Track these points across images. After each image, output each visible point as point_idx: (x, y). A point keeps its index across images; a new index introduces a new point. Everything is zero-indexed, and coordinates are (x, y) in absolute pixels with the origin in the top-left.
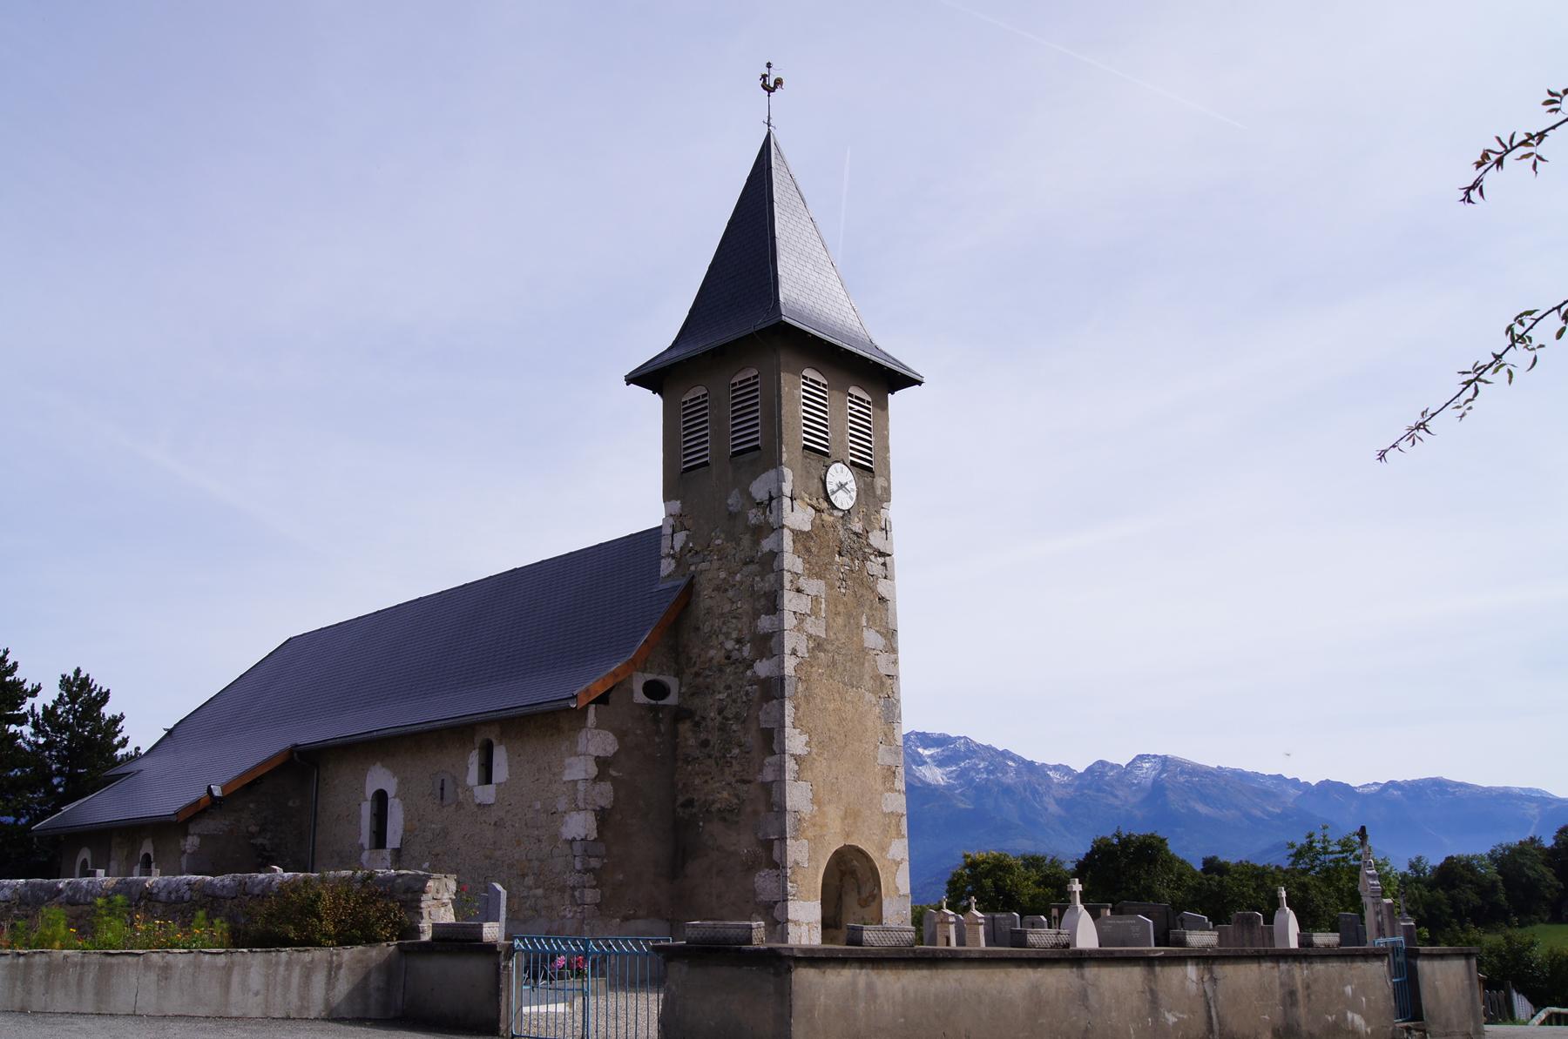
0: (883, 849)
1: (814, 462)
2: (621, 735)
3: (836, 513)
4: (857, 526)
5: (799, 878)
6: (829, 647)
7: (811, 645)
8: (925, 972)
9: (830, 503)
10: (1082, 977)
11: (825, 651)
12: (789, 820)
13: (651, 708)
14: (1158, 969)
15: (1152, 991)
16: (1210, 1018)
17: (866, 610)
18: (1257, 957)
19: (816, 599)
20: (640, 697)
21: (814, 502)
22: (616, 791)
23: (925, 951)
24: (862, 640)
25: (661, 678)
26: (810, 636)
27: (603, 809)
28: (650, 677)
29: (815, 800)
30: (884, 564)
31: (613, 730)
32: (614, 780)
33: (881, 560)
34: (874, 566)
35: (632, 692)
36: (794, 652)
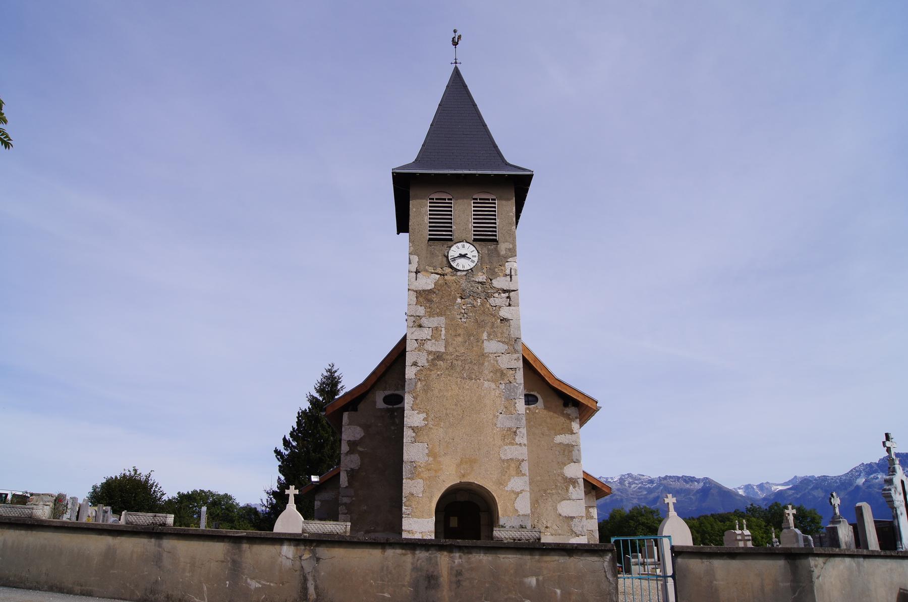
0: (501, 483)
1: (438, 247)
2: (366, 427)
3: (459, 273)
4: (481, 277)
5: (414, 504)
6: (448, 357)
7: (431, 357)
8: (23, 532)
9: (451, 267)
10: (160, 546)
11: (443, 360)
12: (406, 469)
13: (388, 410)
14: (245, 546)
15: (234, 562)
16: (305, 589)
17: (488, 329)
18: (383, 545)
19: (436, 329)
20: (380, 404)
21: (439, 271)
22: (362, 459)
23: (185, 530)
24: (482, 348)
25: (396, 392)
26: (430, 353)
27: (352, 470)
28: (388, 393)
29: (432, 454)
30: (508, 297)
31: (360, 426)
32: (360, 453)
33: (507, 295)
34: (498, 300)
35: (375, 403)
36: (415, 364)
